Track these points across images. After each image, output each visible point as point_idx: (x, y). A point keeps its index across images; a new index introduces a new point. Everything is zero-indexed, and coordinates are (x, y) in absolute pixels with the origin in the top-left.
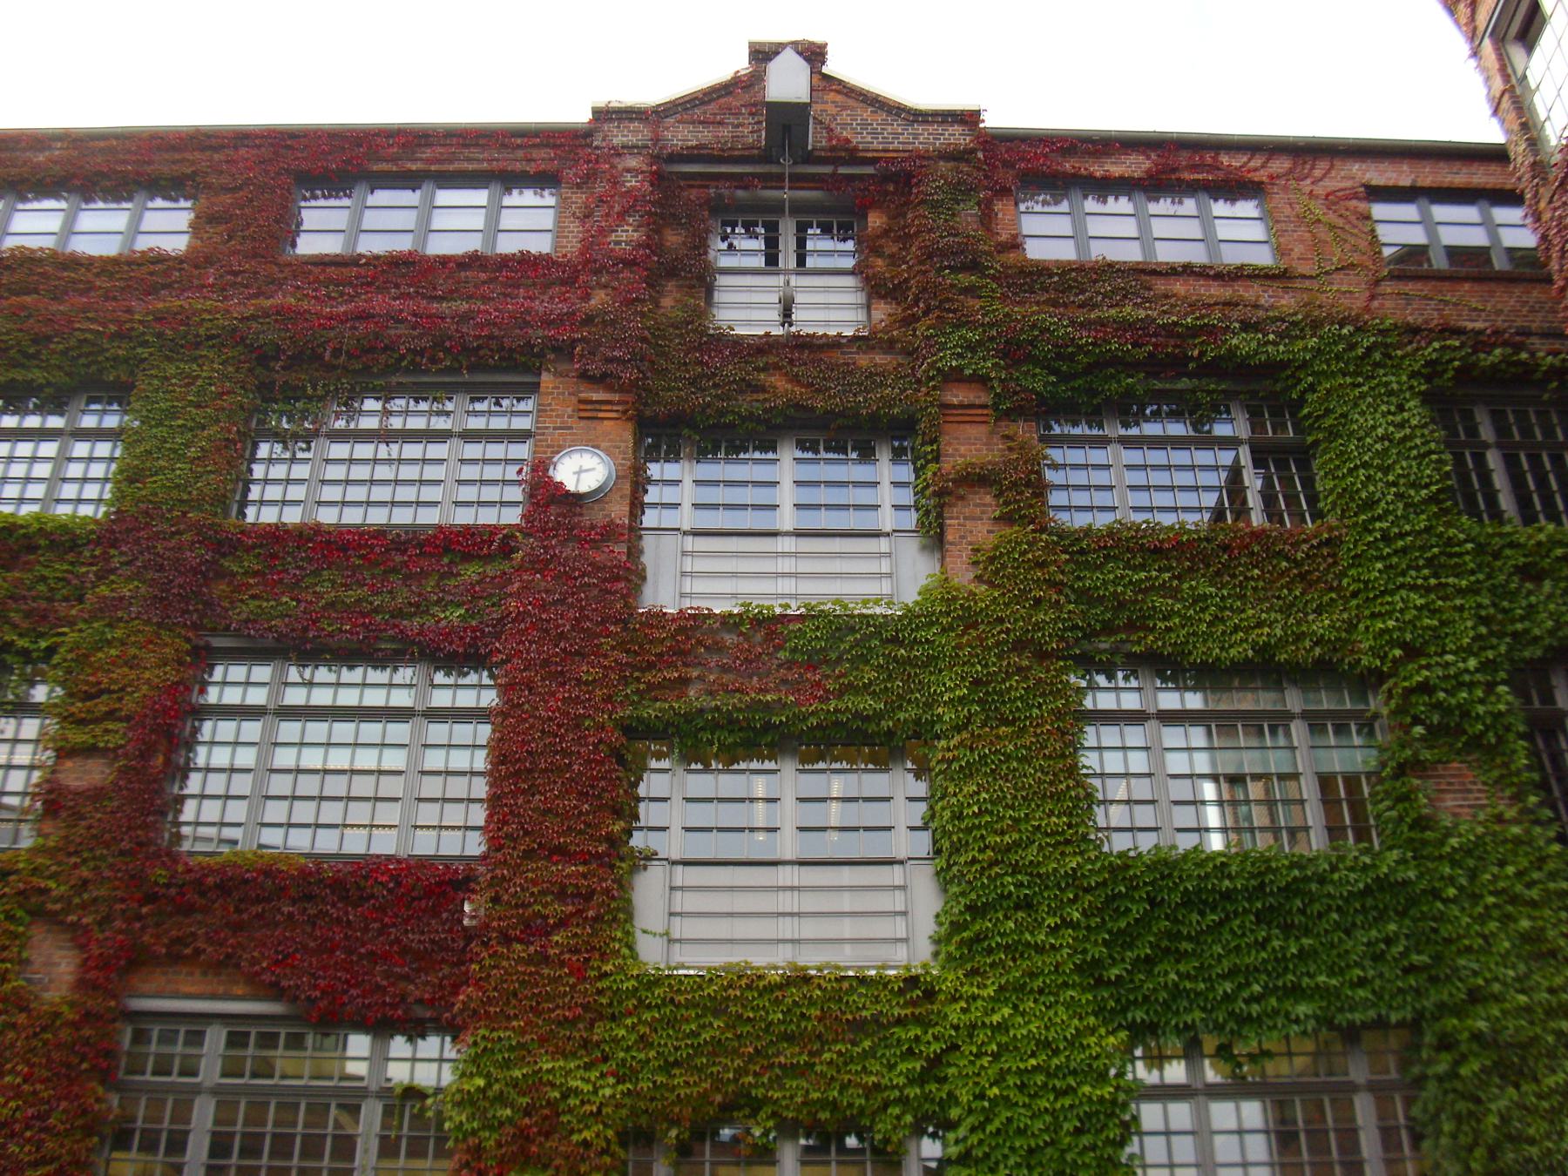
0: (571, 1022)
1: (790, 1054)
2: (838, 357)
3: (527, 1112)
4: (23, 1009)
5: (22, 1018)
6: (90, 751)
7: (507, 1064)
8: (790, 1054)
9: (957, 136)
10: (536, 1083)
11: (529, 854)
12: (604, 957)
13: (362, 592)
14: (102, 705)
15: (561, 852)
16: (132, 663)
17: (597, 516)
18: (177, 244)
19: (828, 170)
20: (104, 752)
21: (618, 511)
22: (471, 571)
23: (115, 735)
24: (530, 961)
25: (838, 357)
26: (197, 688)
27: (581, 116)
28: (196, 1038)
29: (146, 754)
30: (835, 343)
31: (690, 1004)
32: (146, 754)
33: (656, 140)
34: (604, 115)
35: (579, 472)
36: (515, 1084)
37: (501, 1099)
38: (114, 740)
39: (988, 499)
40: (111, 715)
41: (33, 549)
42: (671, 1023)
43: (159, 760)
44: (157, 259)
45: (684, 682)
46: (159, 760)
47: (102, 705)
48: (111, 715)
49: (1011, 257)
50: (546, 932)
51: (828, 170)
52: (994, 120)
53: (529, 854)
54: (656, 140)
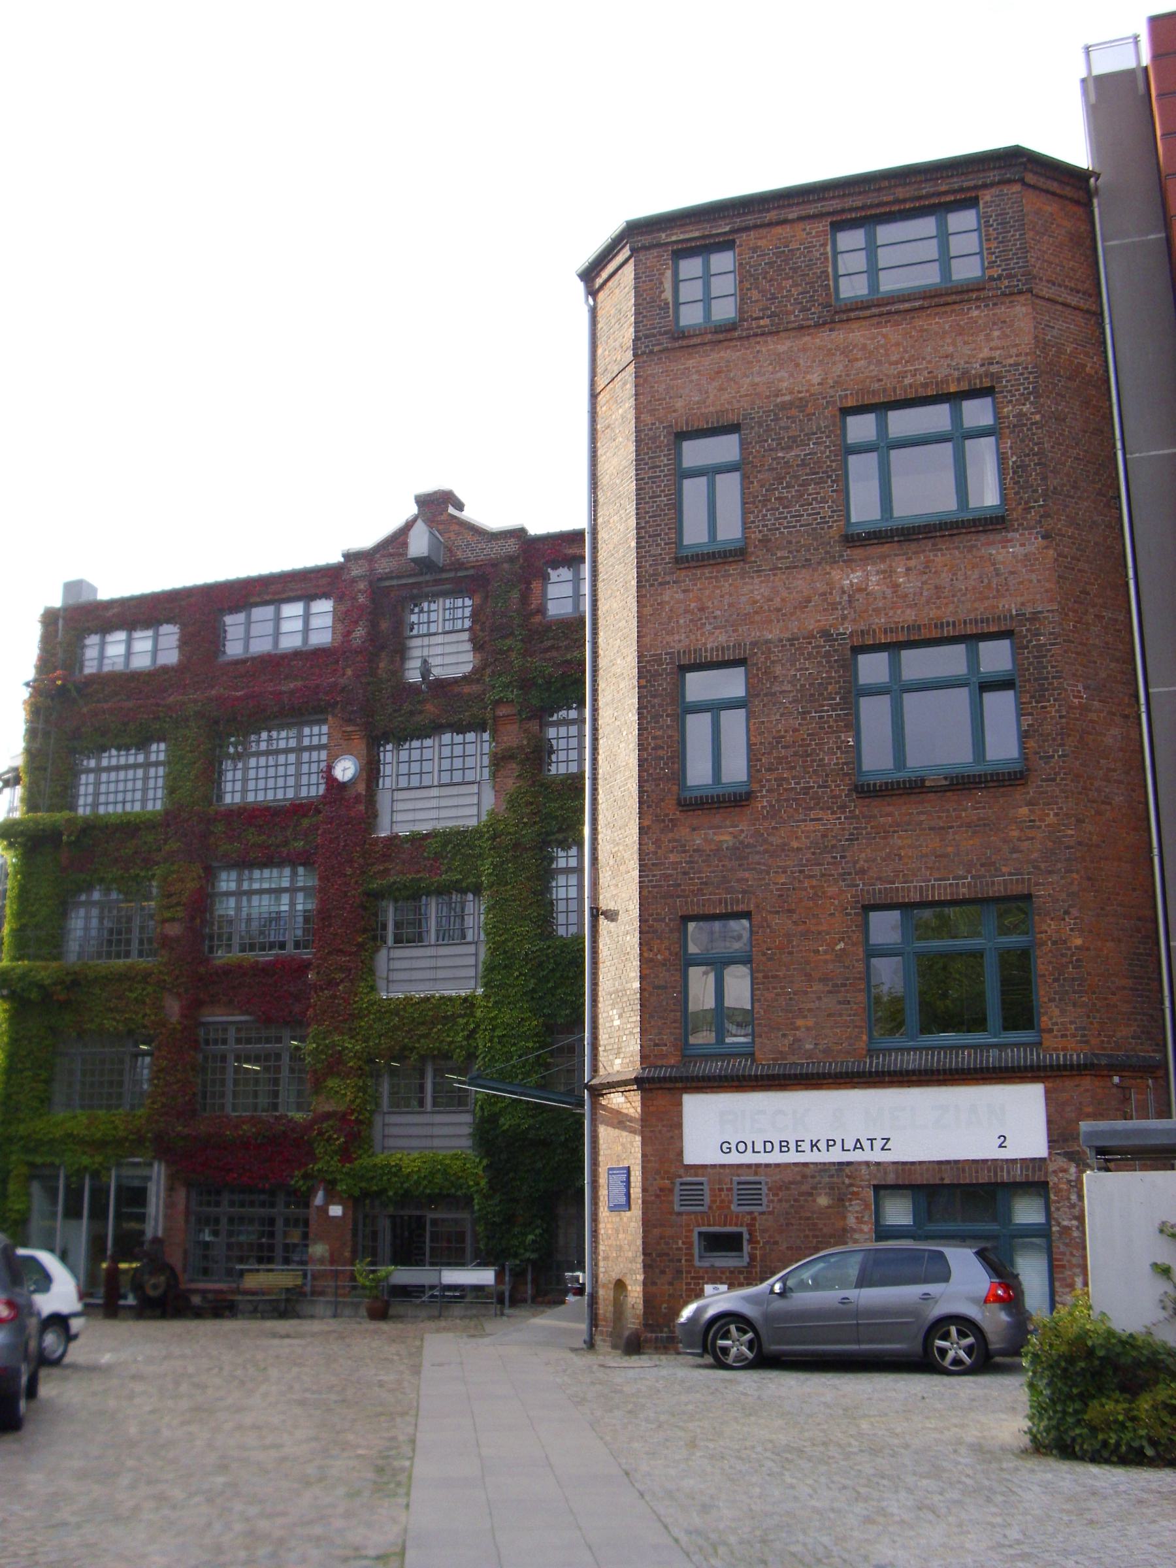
0: (345, 1021)
1: (423, 1030)
2: (456, 689)
3: (332, 1056)
4: (164, 1026)
5: (164, 1030)
6: (173, 919)
7: (324, 1039)
8: (423, 1030)
9: (512, 547)
10: (334, 1045)
11: (330, 953)
12: (356, 995)
13: (264, 837)
14: (174, 900)
15: (340, 952)
16: (182, 880)
17: (351, 793)
18: (170, 657)
19: (452, 575)
20: (178, 920)
21: (361, 788)
22: (306, 822)
23: (180, 913)
24: (331, 997)
25: (456, 689)
26: (451, 510)
27: (336, 558)
28: (225, 1030)
29: (193, 919)
30: (456, 681)
31: (386, 1012)
32: (193, 919)
33: (372, 570)
34: (349, 557)
35: (344, 770)
36: (327, 1046)
37: (322, 1052)
38: (181, 915)
39: (514, 766)
40: (178, 904)
41: (140, 829)
42: (380, 1019)
43: (198, 921)
44: (165, 669)
45: (387, 871)
46: (198, 921)
47: (174, 900)
48: (178, 904)
49: (537, 619)
50: (338, 984)
51: (452, 575)
52: (536, 528)
53: (330, 953)
54: (372, 570)
